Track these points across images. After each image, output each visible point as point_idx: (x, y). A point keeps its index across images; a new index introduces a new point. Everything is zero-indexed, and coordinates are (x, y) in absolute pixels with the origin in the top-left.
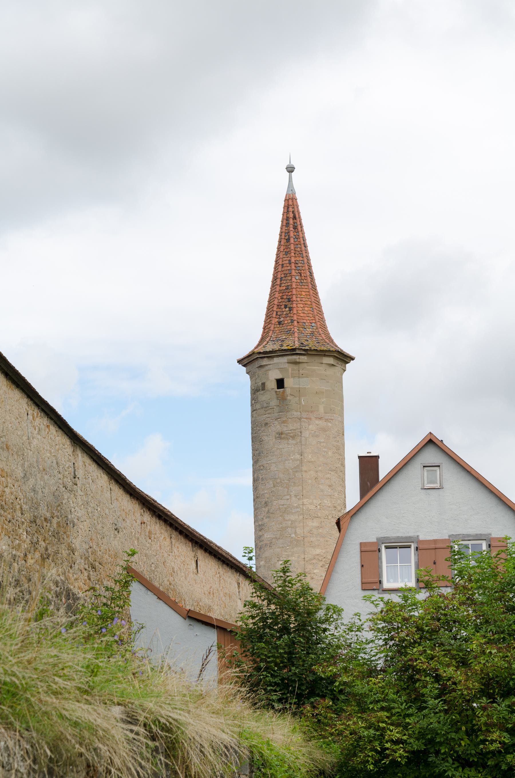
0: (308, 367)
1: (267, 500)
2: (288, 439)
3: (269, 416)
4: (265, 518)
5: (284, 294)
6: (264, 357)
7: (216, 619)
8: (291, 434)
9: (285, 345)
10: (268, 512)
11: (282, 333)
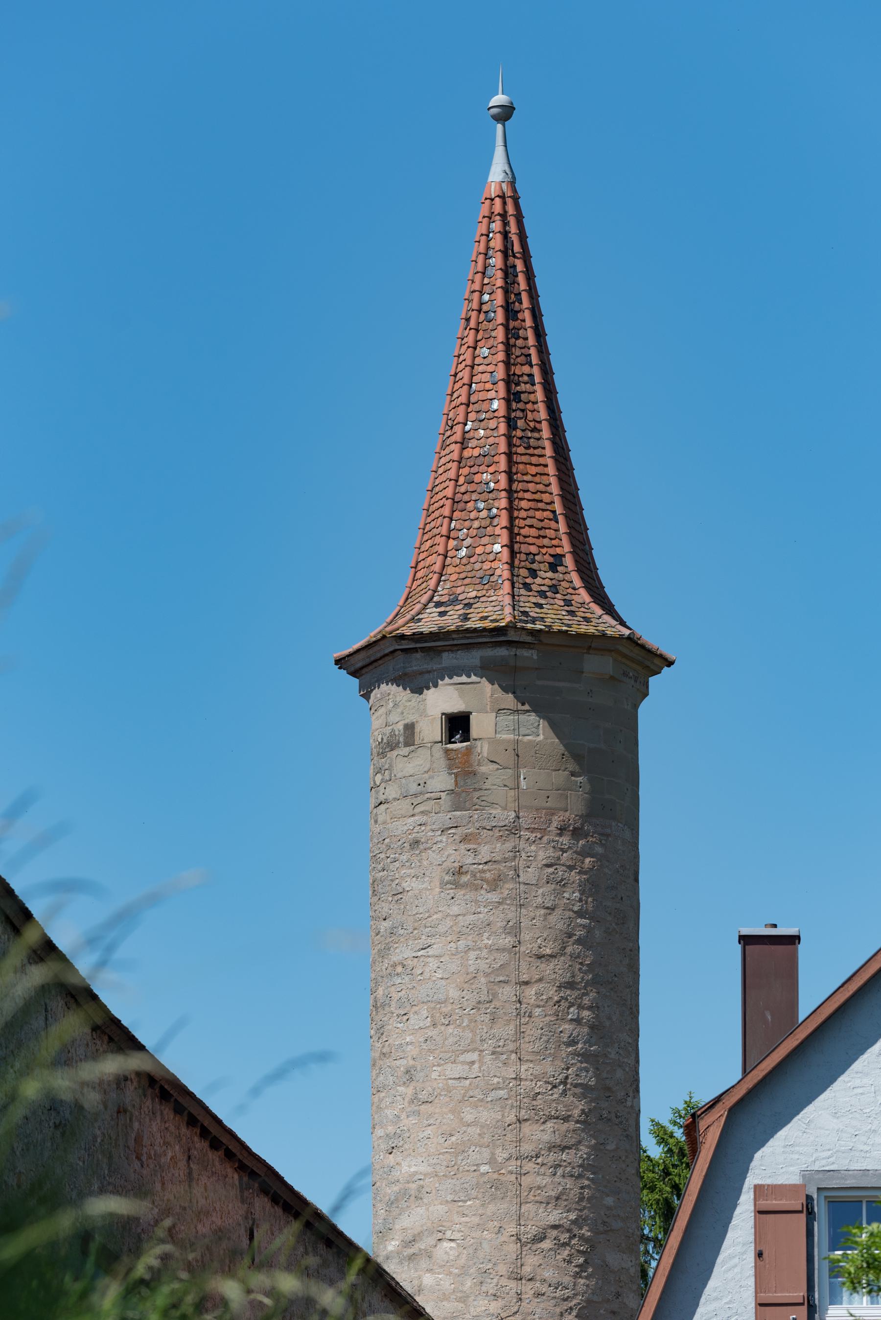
0: (539, 683)
1: (411, 1062)
2: (477, 888)
3: (424, 819)
4: (403, 1116)
6: (415, 650)
8: (488, 875)
9: (475, 617)
11: (467, 581)
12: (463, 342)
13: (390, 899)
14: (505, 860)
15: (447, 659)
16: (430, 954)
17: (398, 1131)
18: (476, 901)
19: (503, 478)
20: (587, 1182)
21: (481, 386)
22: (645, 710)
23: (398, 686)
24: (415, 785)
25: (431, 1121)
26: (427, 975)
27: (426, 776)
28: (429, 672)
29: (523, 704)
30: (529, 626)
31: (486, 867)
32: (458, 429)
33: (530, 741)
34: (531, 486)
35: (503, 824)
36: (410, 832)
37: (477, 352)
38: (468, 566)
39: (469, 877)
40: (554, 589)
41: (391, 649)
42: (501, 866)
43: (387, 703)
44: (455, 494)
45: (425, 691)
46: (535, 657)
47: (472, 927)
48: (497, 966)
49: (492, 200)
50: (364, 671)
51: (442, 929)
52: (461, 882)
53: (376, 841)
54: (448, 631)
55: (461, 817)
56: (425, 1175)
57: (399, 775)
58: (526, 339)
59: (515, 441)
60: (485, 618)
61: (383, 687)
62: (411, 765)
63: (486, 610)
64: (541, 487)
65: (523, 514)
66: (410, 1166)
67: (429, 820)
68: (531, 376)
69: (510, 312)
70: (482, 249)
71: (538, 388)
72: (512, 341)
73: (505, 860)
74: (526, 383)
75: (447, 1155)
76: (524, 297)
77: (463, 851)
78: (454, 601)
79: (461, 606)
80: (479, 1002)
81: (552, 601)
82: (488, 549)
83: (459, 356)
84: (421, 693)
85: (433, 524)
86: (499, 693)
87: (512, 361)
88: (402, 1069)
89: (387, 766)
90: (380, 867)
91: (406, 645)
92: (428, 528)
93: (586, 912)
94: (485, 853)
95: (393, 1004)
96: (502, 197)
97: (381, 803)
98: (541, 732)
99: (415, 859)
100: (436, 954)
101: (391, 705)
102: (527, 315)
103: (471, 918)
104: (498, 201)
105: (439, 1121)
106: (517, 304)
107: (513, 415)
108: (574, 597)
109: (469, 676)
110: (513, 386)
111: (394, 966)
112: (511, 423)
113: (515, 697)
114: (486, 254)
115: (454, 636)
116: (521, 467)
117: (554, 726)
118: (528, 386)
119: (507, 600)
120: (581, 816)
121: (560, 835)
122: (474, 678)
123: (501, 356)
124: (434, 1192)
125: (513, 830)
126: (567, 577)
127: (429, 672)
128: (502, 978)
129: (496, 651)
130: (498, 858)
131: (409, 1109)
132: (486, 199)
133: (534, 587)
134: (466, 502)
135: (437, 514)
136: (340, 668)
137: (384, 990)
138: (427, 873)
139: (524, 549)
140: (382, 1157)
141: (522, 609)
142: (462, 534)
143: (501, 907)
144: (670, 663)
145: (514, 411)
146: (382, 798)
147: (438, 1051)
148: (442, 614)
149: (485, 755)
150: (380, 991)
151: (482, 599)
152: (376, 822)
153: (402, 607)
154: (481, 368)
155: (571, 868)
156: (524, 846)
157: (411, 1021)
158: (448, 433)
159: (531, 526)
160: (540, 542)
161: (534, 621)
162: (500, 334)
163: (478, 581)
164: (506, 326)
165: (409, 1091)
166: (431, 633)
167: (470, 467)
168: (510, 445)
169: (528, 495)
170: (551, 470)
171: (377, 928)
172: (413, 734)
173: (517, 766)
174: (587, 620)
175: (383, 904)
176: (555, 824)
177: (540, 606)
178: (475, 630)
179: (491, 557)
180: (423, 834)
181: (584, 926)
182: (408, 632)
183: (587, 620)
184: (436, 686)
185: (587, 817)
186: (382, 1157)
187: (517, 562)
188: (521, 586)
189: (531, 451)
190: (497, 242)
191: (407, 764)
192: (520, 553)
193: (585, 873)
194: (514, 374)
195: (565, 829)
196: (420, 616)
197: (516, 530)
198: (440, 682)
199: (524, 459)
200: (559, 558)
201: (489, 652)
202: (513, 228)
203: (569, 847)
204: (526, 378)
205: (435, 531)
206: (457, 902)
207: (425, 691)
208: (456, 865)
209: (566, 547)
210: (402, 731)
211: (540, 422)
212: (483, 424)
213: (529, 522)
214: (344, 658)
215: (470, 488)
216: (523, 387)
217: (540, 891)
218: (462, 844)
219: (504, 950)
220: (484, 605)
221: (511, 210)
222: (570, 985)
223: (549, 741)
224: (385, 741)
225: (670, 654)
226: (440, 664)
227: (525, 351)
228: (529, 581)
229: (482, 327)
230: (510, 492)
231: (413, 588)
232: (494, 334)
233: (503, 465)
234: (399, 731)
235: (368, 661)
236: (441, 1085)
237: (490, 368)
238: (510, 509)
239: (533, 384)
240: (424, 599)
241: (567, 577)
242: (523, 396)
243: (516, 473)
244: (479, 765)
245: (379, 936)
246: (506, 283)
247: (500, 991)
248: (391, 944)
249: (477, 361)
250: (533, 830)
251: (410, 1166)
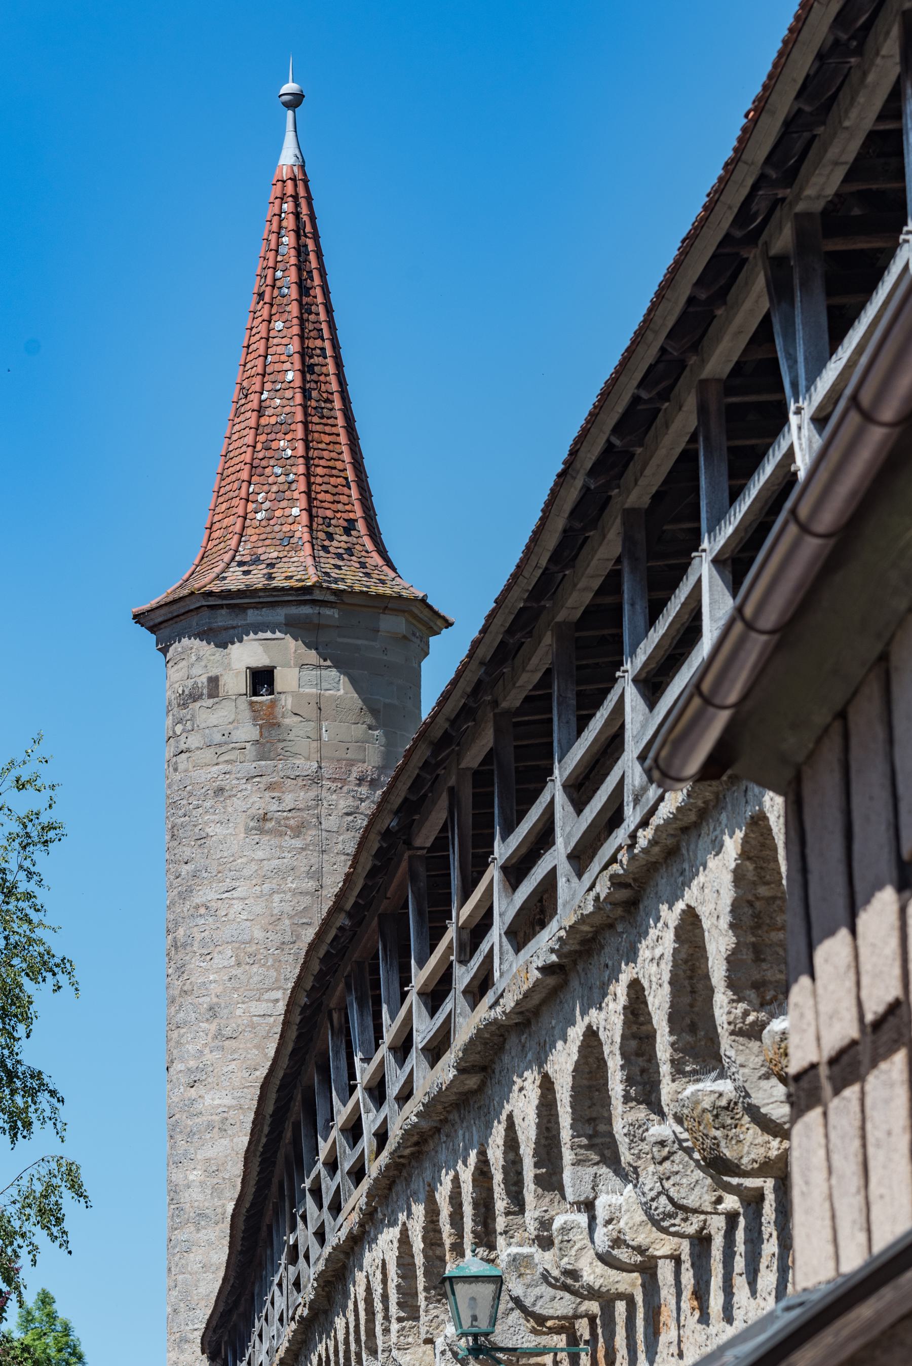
0: (340, 640)
1: (215, 1000)
2: (282, 834)
3: (228, 767)
4: (207, 1051)
6: (221, 606)
7: (440, 832)
8: (292, 822)
10: (218, 1035)
11: (268, 542)
12: (256, 316)
13: (193, 843)
14: (308, 808)
15: (252, 616)
16: (235, 896)
17: (201, 1065)
18: (281, 847)
19: (300, 445)
21: (276, 358)
23: (202, 640)
24: (220, 735)
25: (236, 1056)
26: (231, 917)
27: (231, 726)
28: (234, 628)
29: (325, 660)
30: (333, 586)
31: (290, 815)
32: (254, 397)
33: (332, 695)
34: (326, 454)
35: (307, 773)
37: (271, 325)
38: (268, 528)
39: (273, 823)
41: (198, 605)
42: (305, 814)
43: (189, 656)
44: (253, 459)
45: (230, 646)
46: (336, 616)
47: (277, 871)
49: (284, 182)
50: (162, 626)
51: (246, 872)
52: (266, 828)
53: (176, 788)
54: (256, 589)
55: (266, 767)
56: (229, 1107)
57: (202, 725)
58: (318, 314)
61: (185, 641)
62: (215, 716)
63: (290, 570)
64: (334, 455)
65: (319, 480)
66: (213, 1099)
67: (234, 769)
68: (323, 349)
70: (275, 227)
71: (330, 361)
72: (305, 316)
73: (308, 808)
74: (318, 356)
75: (251, 1089)
76: (315, 274)
77: (268, 799)
78: (257, 561)
79: (264, 566)
80: (283, 943)
81: (348, 563)
83: (251, 329)
84: (225, 647)
85: (228, 488)
86: (303, 649)
87: (306, 335)
88: (205, 1006)
89: (189, 717)
90: (181, 813)
91: (212, 601)
92: (222, 491)
94: (289, 800)
95: (196, 944)
96: (294, 179)
97: (182, 752)
98: (341, 687)
99: (220, 806)
100: (241, 896)
101: (194, 658)
102: (318, 291)
103: (275, 862)
104: (289, 183)
105: (243, 1056)
106: (309, 281)
107: (308, 386)
108: (367, 560)
109: (274, 633)
110: (307, 358)
111: (197, 907)
112: (306, 394)
113: (318, 653)
114: (279, 233)
115: (261, 594)
116: (316, 435)
117: (353, 681)
118: (321, 359)
119: (310, 561)
120: (377, 768)
121: (359, 785)
122: (278, 635)
123: (296, 330)
124: (238, 1124)
125: (315, 779)
126: (360, 541)
127: (234, 628)
128: (305, 920)
129: (300, 609)
130: (301, 806)
131: (213, 1044)
132: (278, 181)
133: (331, 549)
134: (264, 468)
135: (233, 478)
136: (136, 623)
137: (185, 931)
138: (232, 819)
139: (321, 512)
140: (182, 1090)
141: (323, 570)
142: (260, 498)
143: (304, 853)
144: (449, 624)
145: (309, 382)
146: (183, 747)
147: (242, 990)
148: (246, 573)
149: (289, 707)
150: (181, 931)
151: (284, 560)
152: (176, 770)
153: (197, 566)
154: (276, 341)
156: (326, 795)
157: (215, 961)
158: (243, 401)
159: (326, 492)
160: (333, 507)
161: (336, 581)
162: (294, 309)
163: (278, 542)
164: (300, 302)
165: (213, 1027)
166: (239, 590)
167: (268, 434)
168: (306, 414)
169: (322, 462)
170: (343, 439)
171: (177, 871)
172: (217, 686)
174: (383, 582)
175: (185, 849)
176: (354, 775)
177: (339, 567)
178: (283, 589)
179: (290, 520)
180: (229, 782)
182: (216, 589)
183: (383, 582)
184: (241, 641)
186: (182, 1090)
187: (315, 526)
188: (320, 548)
189: (324, 421)
191: (211, 716)
192: (317, 516)
194: (308, 347)
195: (363, 780)
196: (224, 575)
198: (245, 638)
200: (352, 522)
201: (294, 610)
202: (304, 210)
203: (367, 797)
204: (318, 351)
205: (231, 494)
206: (262, 847)
207: (230, 646)
208: (261, 812)
209: (359, 513)
210: (206, 684)
211: (332, 394)
212: (278, 394)
213: (324, 487)
214: (143, 613)
216: (316, 360)
217: (341, 838)
218: (267, 792)
219: (307, 893)
220: (286, 565)
221: (302, 192)
223: (349, 695)
224: (187, 692)
225: (451, 618)
226: (245, 620)
228: (327, 543)
230: (307, 458)
231: (209, 547)
232: (288, 309)
233: (300, 434)
234: (203, 683)
235: (170, 616)
236: (245, 1021)
237: (285, 341)
238: (308, 475)
239: (325, 358)
240: (227, 557)
241: (360, 541)
242: (316, 369)
243: (312, 441)
244: (283, 717)
245: (179, 879)
246: (299, 260)
247: (303, 933)
248: (194, 887)
249: (272, 334)
250: (334, 780)
251: (213, 1099)
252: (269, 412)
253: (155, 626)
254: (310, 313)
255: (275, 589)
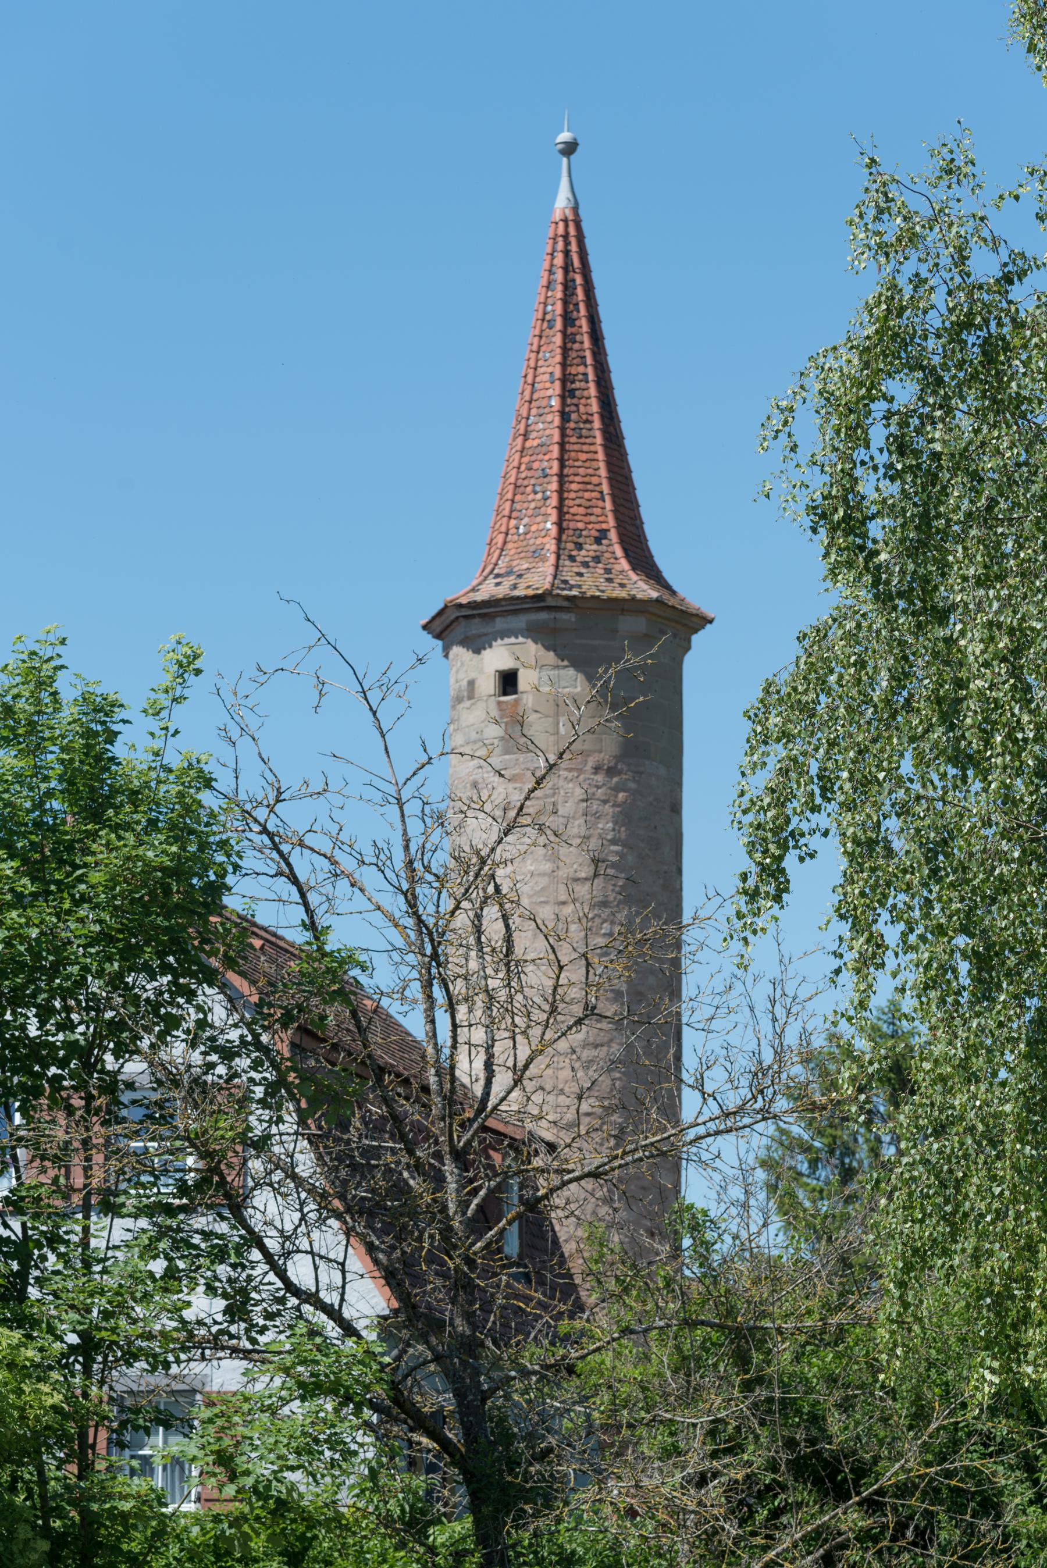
0: (578, 641)
5: (534, 458)
6: (473, 616)
9: (522, 586)
15: (500, 623)
20: (618, 1075)
22: (690, 662)
28: (486, 635)
30: (565, 593)
34: (581, 471)
36: (470, 774)
40: (597, 559)
48: (537, 888)
58: (582, 343)
59: (568, 432)
60: (529, 587)
65: (572, 495)
68: (585, 374)
69: (568, 319)
72: (569, 345)
76: (582, 307)
78: (509, 573)
82: (541, 526)
86: (542, 652)
93: (619, 840)
96: (565, 221)
104: (561, 225)
107: (567, 409)
112: (565, 416)
116: (573, 454)
120: (615, 757)
121: (595, 773)
122: (521, 639)
123: (558, 358)
126: (610, 549)
127: (486, 635)
139: (572, 525)
148: (498, 584)
155: (605, 802)
162: (558, 339)
169: (578, 479)
173: (557, 715)
174: (622, 585)
177: (581, 575)
179: (543, 533)
181: (617, 853)
183: (622, 585)
184: (491, 646)
185: (620, 758)
187: (564, 537)
189: (583, 440)
190: (559, 260)
193: (619, 806)
197: (565, 509)
199: (576, 447)
204: (580, 377)
215: (530, 474)
216: (577, 385)
221: (572, 231)
222: (604, 904)
227: (581, 354)
228: (574, 553)
229: (545, 334)
230: (561, 476)
237: (550, 369)
238: (561, 491)
239: (587, 382)
241: (610, 549)
242: (577, 393)
249: (540, 363)
252: (533, 435)
253: (442, 632)
254: (575, 342)
255: (518, 598)
